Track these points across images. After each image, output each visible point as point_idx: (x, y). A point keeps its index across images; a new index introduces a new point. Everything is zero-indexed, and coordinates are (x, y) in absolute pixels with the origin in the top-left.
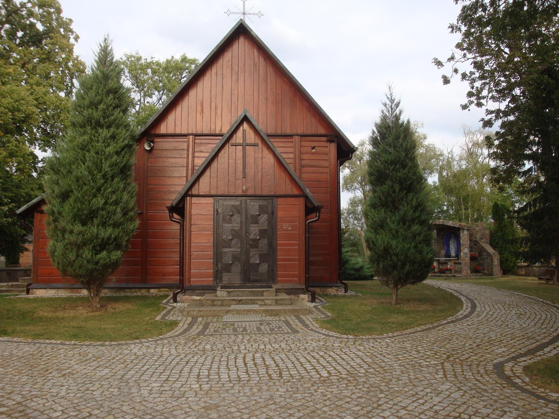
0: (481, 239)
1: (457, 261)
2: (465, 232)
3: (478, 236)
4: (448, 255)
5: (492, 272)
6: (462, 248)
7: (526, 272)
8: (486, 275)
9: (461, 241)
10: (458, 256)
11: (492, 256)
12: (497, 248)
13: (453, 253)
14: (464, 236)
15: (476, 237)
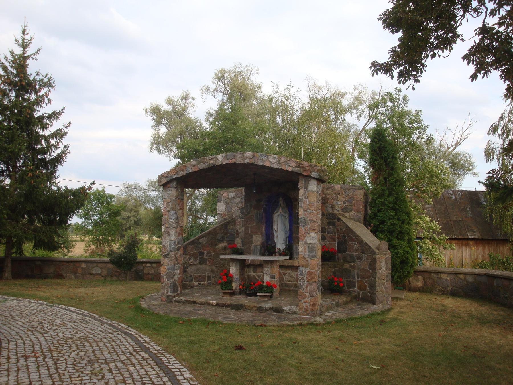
0: (345, 210)
1: (290, 263)
2: (313, 186)
3: (339, 204)
4: (269, 248)
5: (373, 293)
6: (302, 230)
7: (425, 283)
8: (356, 298)
9: (301, 213)
10: (290, 251)
11: (373, 252)
12: (382, 232)
13: (280, 244)
14: (309, 195)
15: (333, 207)
